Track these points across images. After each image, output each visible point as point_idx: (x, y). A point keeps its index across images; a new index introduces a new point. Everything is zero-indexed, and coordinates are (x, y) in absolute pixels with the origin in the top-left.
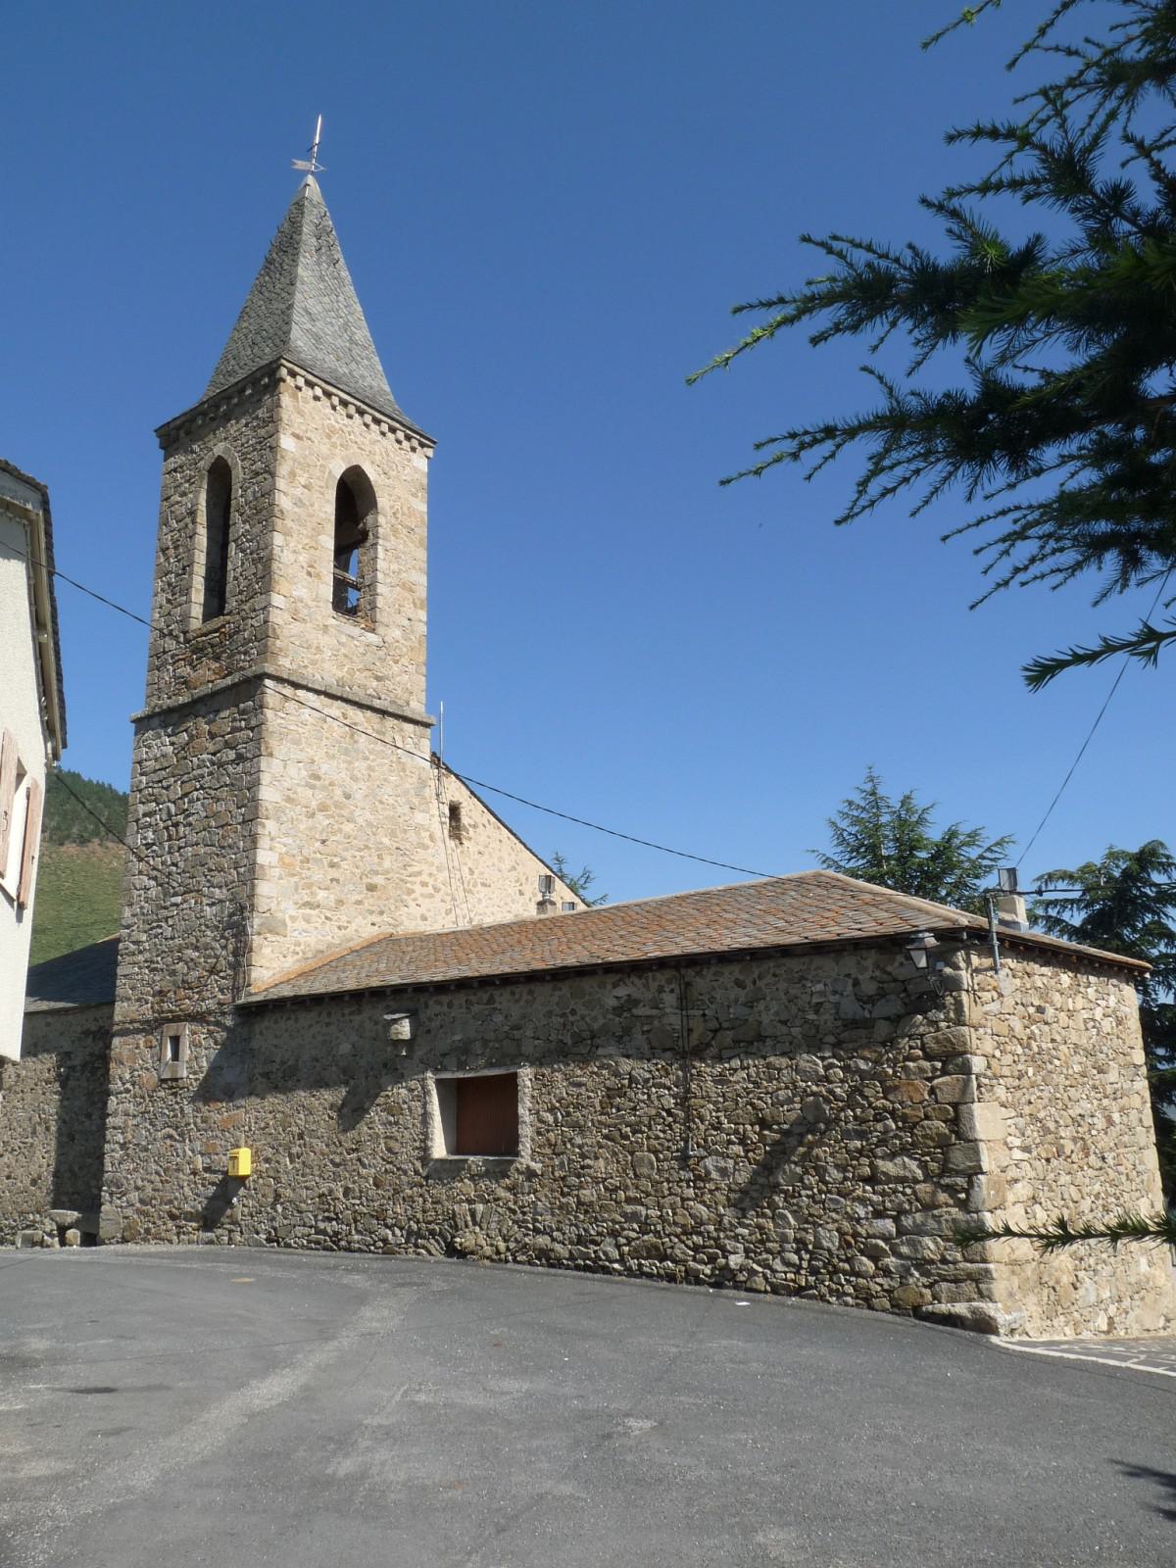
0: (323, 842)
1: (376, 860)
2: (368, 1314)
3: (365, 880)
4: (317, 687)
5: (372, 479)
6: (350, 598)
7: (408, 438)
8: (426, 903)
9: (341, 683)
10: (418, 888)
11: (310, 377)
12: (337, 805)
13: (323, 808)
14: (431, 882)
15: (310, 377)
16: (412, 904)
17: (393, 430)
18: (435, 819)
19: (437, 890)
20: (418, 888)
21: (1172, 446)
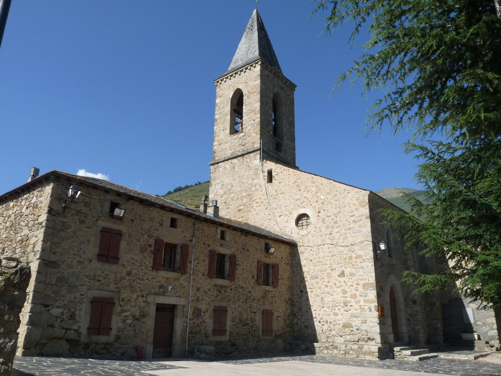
0: (225, 203)
1: (241, 201)
2: (443, 192)
3: (237, 209)
4: (222, 160)
5: (233, 93)
6: (235, 128)
7: (252, 66)
8: (257, 209)
9: (232, 154)
10: (255, 205)
11: (230, 74)
12: (229, 190)
13: (225, 193)
14: (260, 201)
15: (230, 74)
16: (252, 210)
17: (246, 69)
18: (262, 178)
19: (262, 203)
20: (255, 205)
21: (500, 282)
